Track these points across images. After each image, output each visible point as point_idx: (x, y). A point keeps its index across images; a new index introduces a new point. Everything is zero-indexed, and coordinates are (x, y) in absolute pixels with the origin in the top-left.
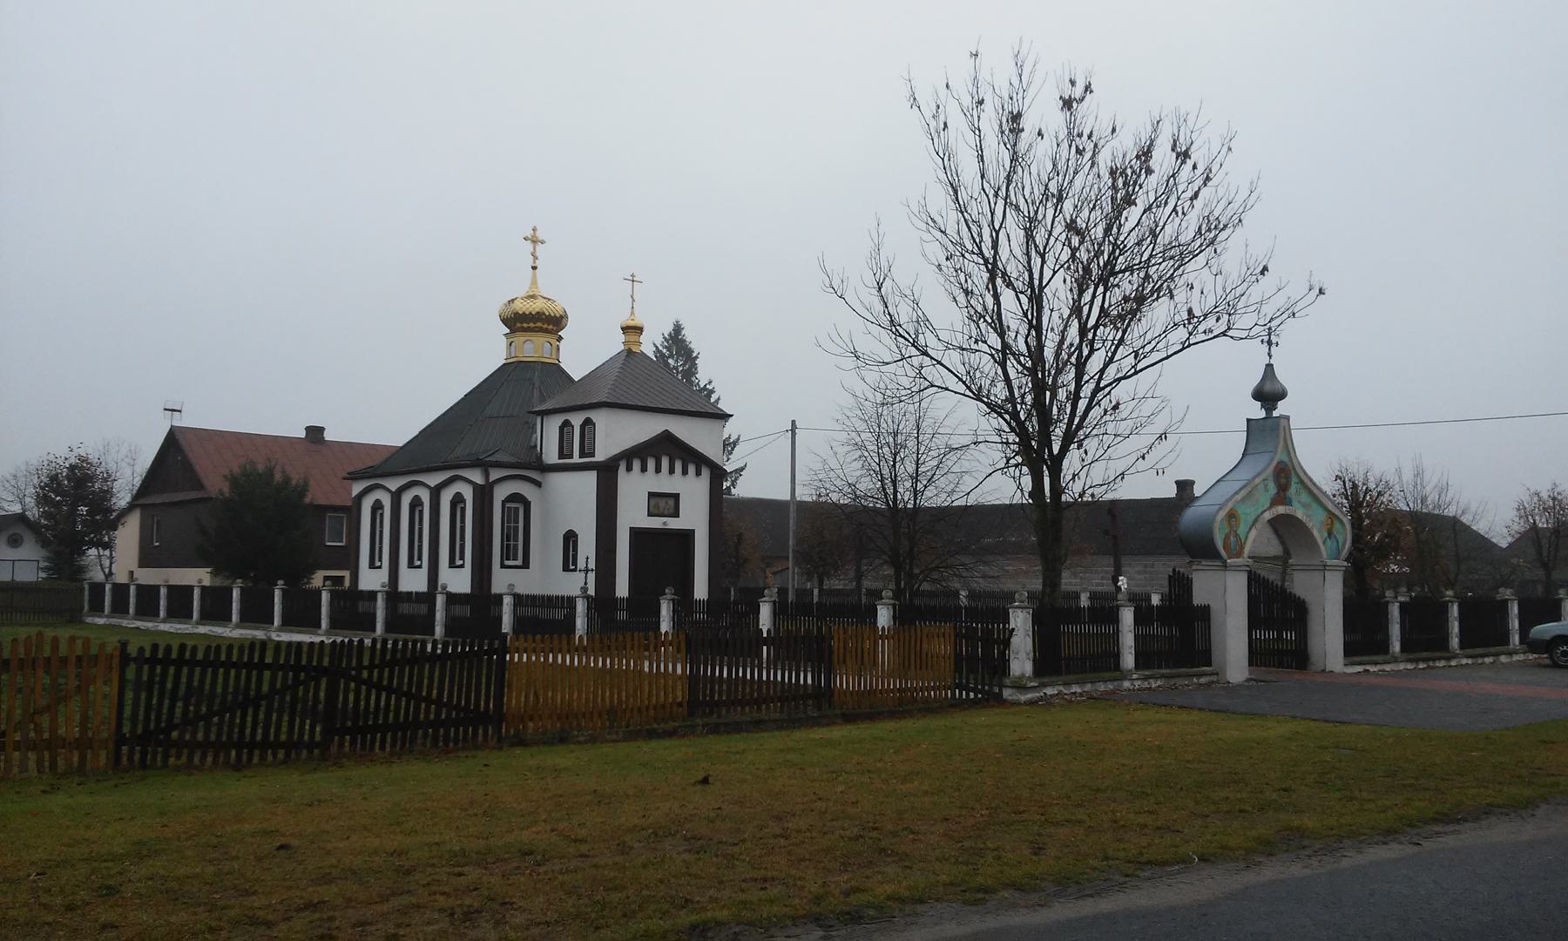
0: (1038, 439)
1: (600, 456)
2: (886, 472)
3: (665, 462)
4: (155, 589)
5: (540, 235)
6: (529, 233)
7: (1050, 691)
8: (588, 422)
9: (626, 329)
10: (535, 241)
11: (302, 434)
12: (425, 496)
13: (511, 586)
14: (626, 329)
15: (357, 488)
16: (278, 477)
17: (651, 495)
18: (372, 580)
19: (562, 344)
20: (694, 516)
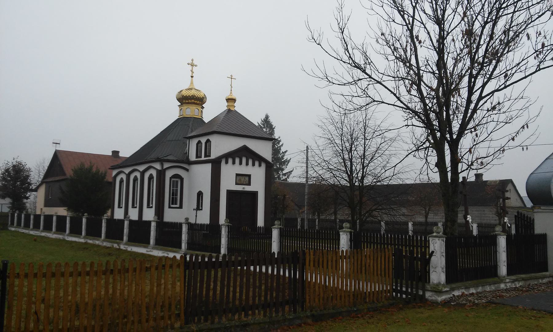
0: (441, 126)
1: (214, 155)
2: (346, 156)
3: (244, 160)
4: (51, 217)
5: (195, 62)
6: (190, 62)
7: (457, 293)
8: (208, 141)
9: (228, 100)
10: (192, 65)
11: (110, 154)
12: (138, 175)
13: (56, 213)
14: (228, 100)
15: (114, 173)
16: (94, 170)
17: (237, 175)
18: (119, 214)
19: (204, 110)
20: (258, 184)
